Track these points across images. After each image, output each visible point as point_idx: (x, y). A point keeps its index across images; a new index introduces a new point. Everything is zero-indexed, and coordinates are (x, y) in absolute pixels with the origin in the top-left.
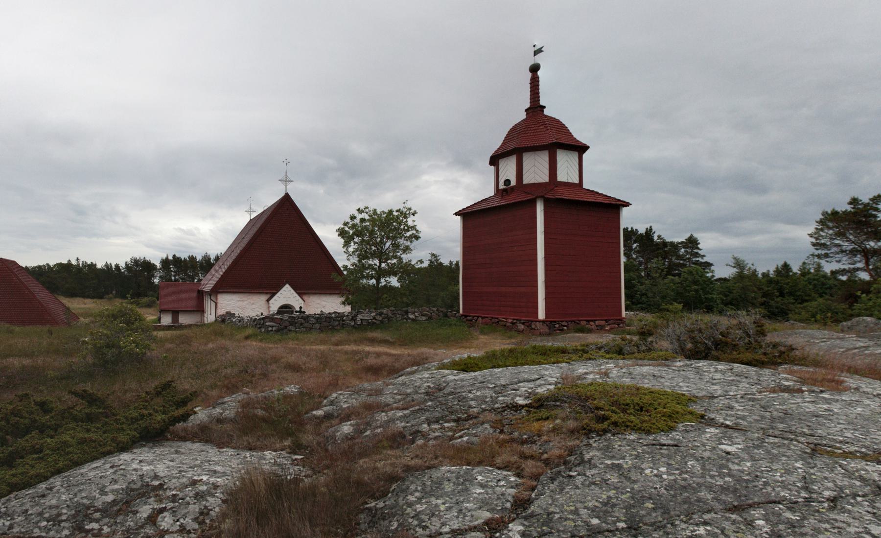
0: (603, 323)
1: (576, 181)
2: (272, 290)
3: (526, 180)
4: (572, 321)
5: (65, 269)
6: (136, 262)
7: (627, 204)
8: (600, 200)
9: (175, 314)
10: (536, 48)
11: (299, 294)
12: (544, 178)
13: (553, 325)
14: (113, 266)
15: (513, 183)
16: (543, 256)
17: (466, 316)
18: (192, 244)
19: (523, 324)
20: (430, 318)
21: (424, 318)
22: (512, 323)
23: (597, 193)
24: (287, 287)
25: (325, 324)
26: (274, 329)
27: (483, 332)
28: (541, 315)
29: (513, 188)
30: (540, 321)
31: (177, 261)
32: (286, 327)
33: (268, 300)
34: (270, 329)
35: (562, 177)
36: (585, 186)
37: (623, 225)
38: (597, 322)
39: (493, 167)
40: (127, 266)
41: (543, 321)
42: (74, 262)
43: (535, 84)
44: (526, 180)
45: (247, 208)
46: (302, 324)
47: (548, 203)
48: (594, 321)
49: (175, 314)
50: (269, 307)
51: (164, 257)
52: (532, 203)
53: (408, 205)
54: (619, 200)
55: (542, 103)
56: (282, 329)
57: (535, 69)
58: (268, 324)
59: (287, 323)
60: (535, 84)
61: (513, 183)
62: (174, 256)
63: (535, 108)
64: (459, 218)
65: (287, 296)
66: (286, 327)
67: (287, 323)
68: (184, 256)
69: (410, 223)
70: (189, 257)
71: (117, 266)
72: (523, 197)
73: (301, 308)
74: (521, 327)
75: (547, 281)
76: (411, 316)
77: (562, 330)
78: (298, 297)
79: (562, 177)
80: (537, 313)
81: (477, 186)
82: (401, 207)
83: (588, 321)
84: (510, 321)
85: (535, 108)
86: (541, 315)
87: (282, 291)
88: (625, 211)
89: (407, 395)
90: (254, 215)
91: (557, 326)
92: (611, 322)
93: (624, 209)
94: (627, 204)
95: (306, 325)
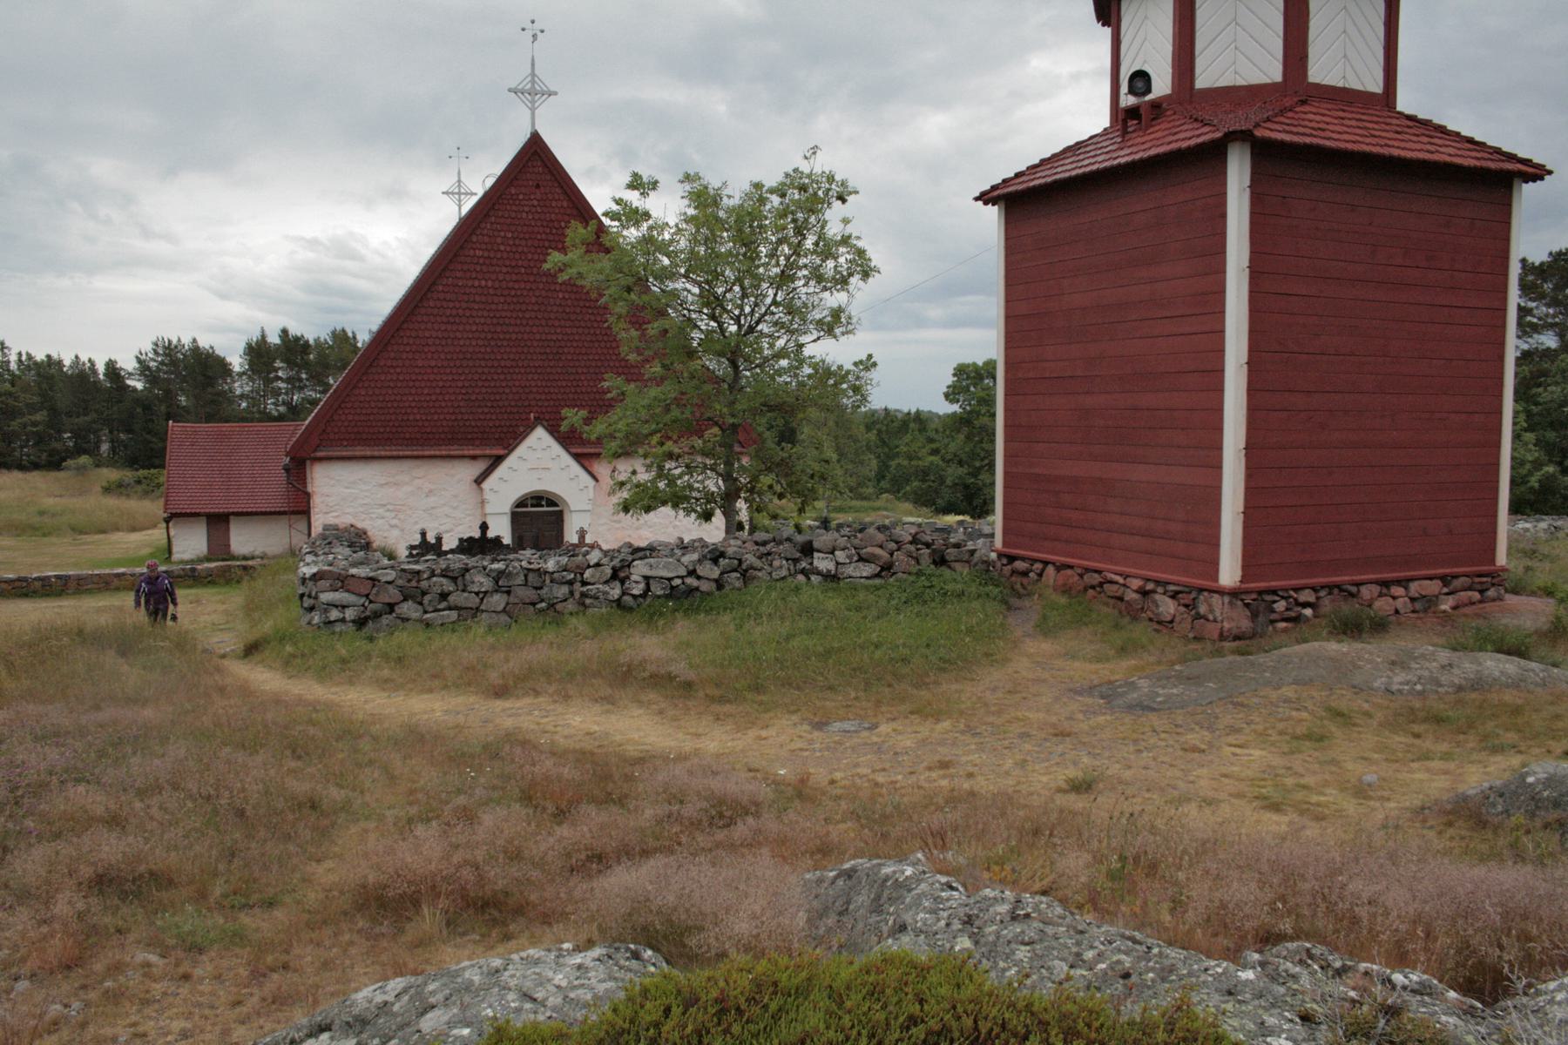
0: (1433, 587)
1: (1375, 85)
2: (490, 442)
3: (1207, 76)
4: (1330, 588)
6: (168, 351)
7: (1537, 173)
8: (1445, 154)
9: (218, 522)
11: (578, 457)
12: (1271, 70)
13: (1267, 608)
14: (67, 362)
15: (1162, 86)
16: (1244, 358)
17: (1012, 559)
18: (363, 285)
19: (1174, 596)
20: (887, 568)
21: (868, 569)
22: (1144, 593)
23: (1442, 130)
24: (540, 440)
25: (529, 594)
26: (350, 614)
27: (1045, 629)
28: (1229, 572)
29: (1156, 105)
30: (1221, 592)
31: (293, 347)
32: (391, 607)
33: (479, 481)
34: (334, 614)
35: (1323, 69)
36: (1406, 102)
37: (599, 212)
38: (1414, 586)
39: (1108, 31)
41: (1234, 594)
42: (175, 341)
44: (1207, 76)
45: (448, 183)
46: (444, 596)
47: (1266, 154)
48: (1404, 583)
49: (218, 522)
50: (483, 502)
51: (255, 336)
52: (1211, 156)
53: (821, 164)
54: (1512, 157)
56: (377, 615)
58: (326, 597)
59: (393, 594)
61: (1162, 86)
62: (285, 332)
66: (391, 607)
68: (313, 330)
69: (834, 230)
70: (334, 333)
71: (112, 369)
72: (1188, 136)
74: (1168, 607)
75: (1252, 449)
76: (823, 563)
77: (1296, 619)
78: (575, 468)
79: (1323, 69)
83: (1385, 584)
84: (1136, 583)
86: (1229, 572)
87: (521, 450)
88: (1528, 193)
89: (877, 784)
90: (466, 209)
91: (1281, 606)
92: (1457, 583)
93: (1528, 189)
94: (1537, 173)
95: (457, 598)
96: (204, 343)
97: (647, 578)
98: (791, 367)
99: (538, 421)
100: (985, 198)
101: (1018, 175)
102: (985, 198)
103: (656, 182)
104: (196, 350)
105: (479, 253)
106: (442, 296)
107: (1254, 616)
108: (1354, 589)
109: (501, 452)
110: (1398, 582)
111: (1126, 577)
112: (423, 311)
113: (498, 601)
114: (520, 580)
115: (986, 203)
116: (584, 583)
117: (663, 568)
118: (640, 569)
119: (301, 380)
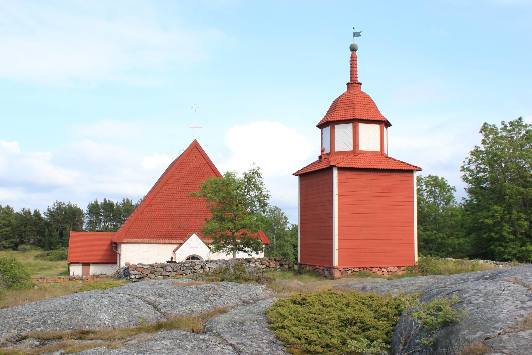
2: (179, 237)
5: (312, 164)
10: (355, 31)
14: (32, 212)
28: (336, 263)
31: (108, 206)
35: (363, 147)
38: (389, 269)
40: (51, 214)
43: (353, 61)
52: (330, 169)
54: (416, 167)
55: (359, 80)
57: (353, 49)
59: (148, 272)
60: (353, 61)
63: (353, 84)
64: (297, 177)
65: (195, 246)
67: (148, 272)
68: (117, 201)
71: (37, 214)
73: (172, 258)
75: (339, 235)
79: (363, 147)
80: (332, 262)
81: (307, 151)
82: (252, 168)
85: (353, 84)
92: (402, 269)
95: (164, 273)
96: (73, 204)
97: (209, 268)
98: (434, 197)
99: (194, 232)
100: (295, 174)
101: (302, 169)
102: (295, 174)
103: (354, 36)
104: (70, 207)
105: (176, 178)
106: (164, 192)
107: (342, 274)
108: (370, 269)
109: (181, 241)
110: (384, 267)
111: (320, 266)
112: (158, 196)
113: (174, 274)
114: (179, 268)
115: (296, 176)
116: (194, 269)
117: (213, 266)
118: (208, 265)
119: (110, 216)
